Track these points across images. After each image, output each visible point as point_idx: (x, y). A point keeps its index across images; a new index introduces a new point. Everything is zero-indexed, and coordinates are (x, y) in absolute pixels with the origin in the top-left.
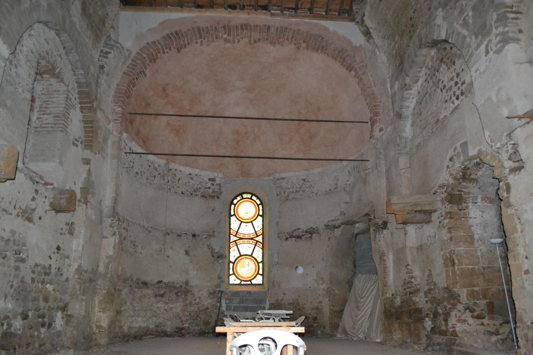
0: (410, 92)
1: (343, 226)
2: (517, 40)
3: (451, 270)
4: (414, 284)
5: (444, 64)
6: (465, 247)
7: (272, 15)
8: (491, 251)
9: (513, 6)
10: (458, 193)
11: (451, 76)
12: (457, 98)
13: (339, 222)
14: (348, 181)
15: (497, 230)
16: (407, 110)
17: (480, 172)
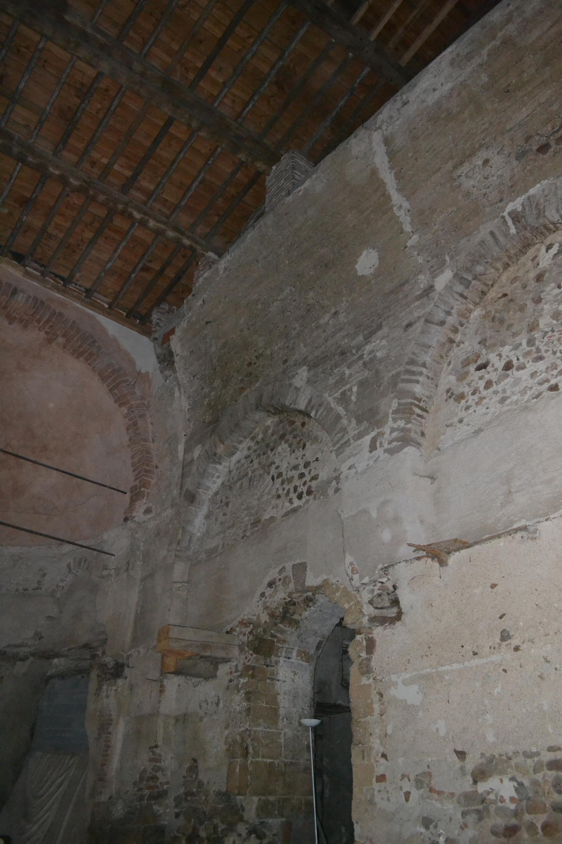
0: (218, 466)
1: (31, 659)
2: (418, 445)
3: (239, 762)
4: (160, 781)
5: (285, 443)
6: (265, 727)
7: (27, 273)
8: (298, 737)
9: (421, 399)
10: (270, 638)
11: (294, 462)
12: (300, 497)
13: (26, 650)
14: (62, 581)
15: (309, 704)
16: (205, 492)
17: (306, 613)
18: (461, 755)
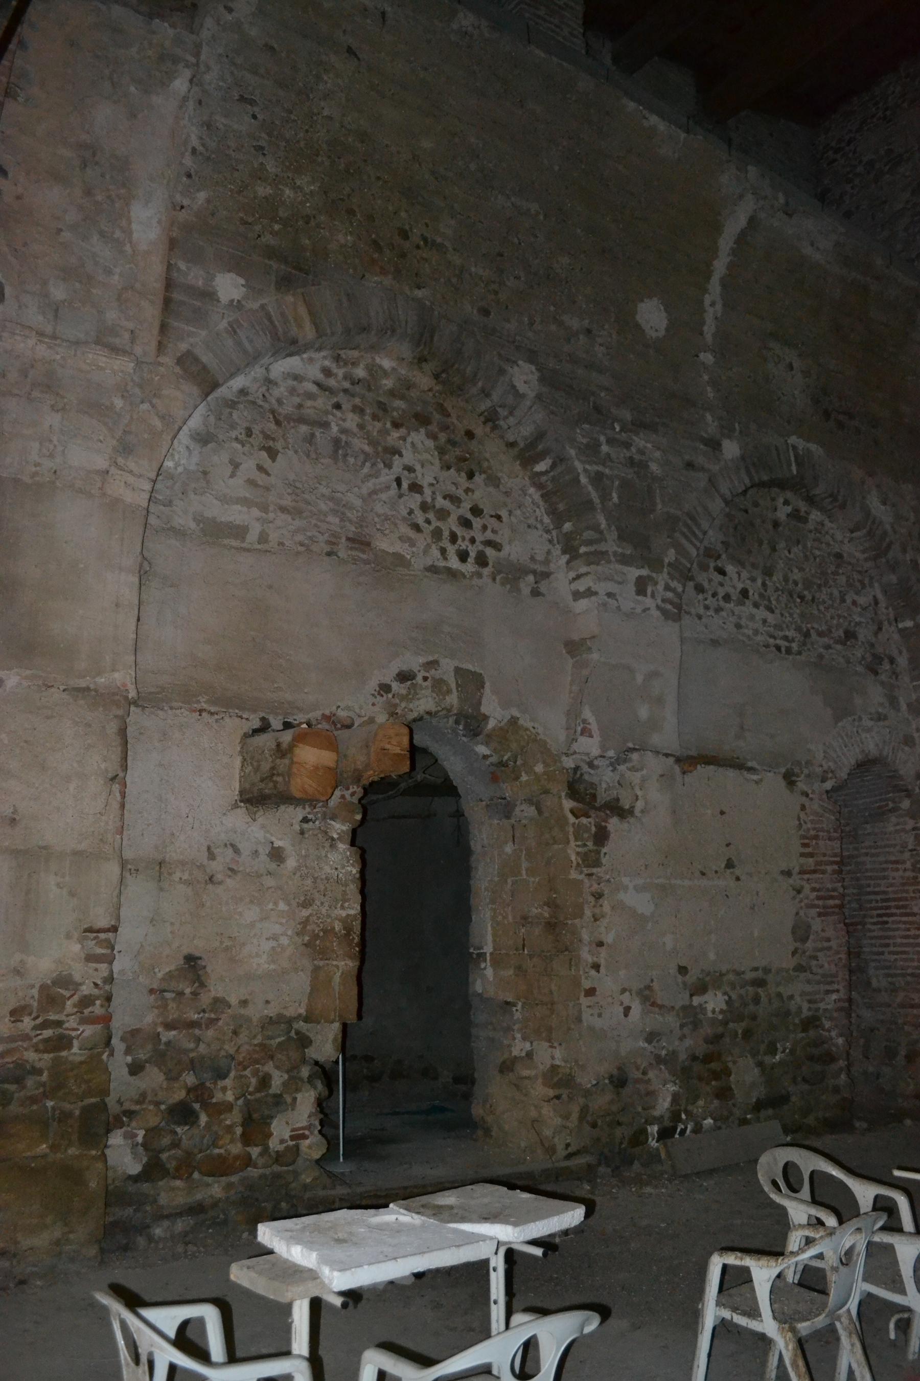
18: (683, 970)
